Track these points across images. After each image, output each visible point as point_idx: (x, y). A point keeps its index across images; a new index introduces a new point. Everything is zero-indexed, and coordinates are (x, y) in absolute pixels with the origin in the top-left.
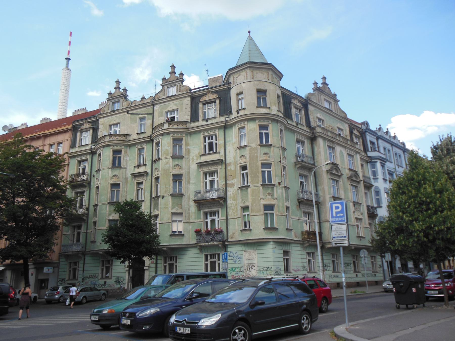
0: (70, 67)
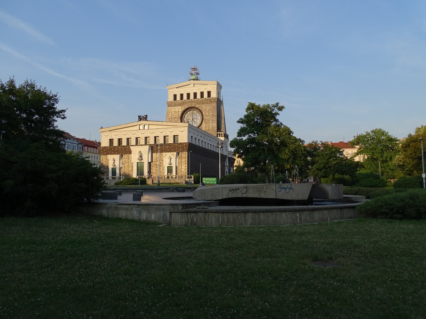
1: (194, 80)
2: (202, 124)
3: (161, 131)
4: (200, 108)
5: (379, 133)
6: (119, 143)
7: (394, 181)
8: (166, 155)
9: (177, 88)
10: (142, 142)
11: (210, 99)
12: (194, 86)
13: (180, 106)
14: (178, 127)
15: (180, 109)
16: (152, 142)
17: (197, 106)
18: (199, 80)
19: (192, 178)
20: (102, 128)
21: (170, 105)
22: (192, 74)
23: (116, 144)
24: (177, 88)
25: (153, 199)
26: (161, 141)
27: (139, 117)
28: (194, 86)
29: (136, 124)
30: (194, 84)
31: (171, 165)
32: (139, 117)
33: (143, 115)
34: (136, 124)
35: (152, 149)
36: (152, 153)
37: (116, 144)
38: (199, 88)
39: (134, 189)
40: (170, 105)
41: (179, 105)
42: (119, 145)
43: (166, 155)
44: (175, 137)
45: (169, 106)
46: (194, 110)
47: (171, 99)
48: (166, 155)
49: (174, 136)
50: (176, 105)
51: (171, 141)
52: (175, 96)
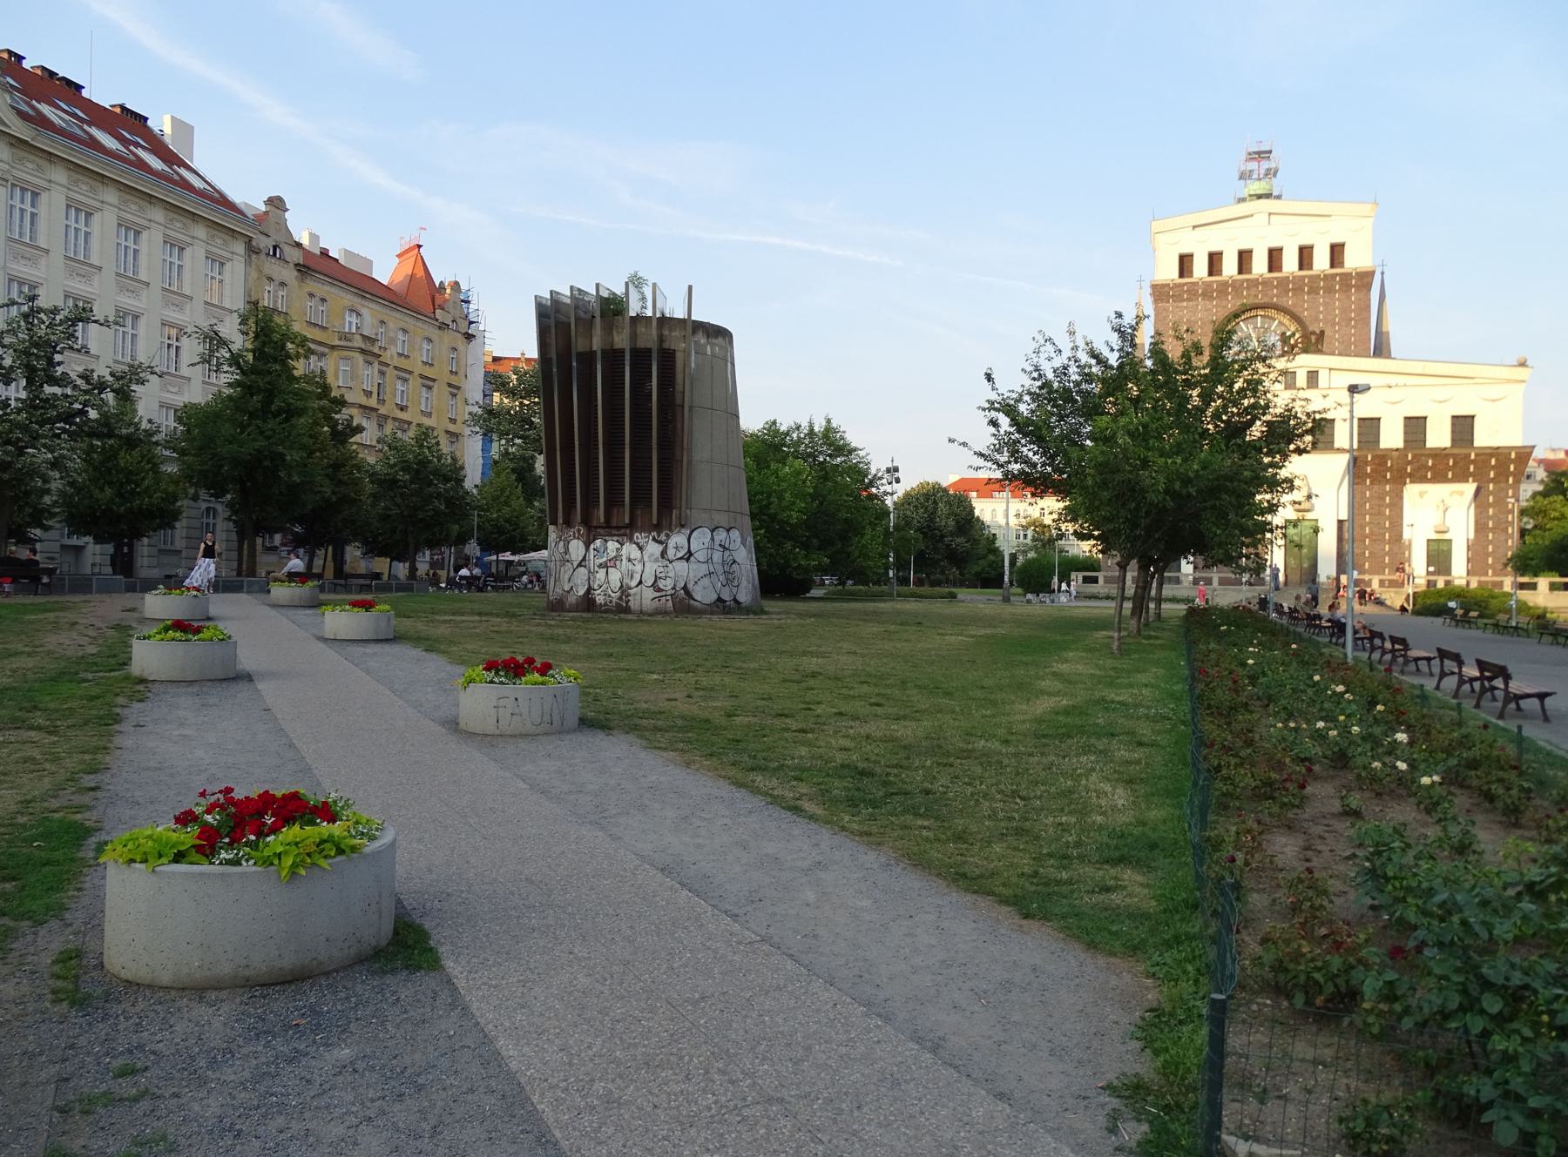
1: (1259, 197)
5: (831, 440)
7: (1479, 582)
9: (1194, 227)
11: (1193, 283)
14: (1475, 381)
18: (1279, 197)
19: (1211, 584)
20: (1523, 364)
22: (1243, 176)
24: (1194, 227)
26: (1392, 437)
30: (1270, 214)
31: (1446, 536)
39: (281, 603)
43: (1426, 492)
44: (1463, 426)
46: (1268, 317)
47: (1169, 272)
48: (1426, 492)
49: (1408, 420)
51: (1439, 436)
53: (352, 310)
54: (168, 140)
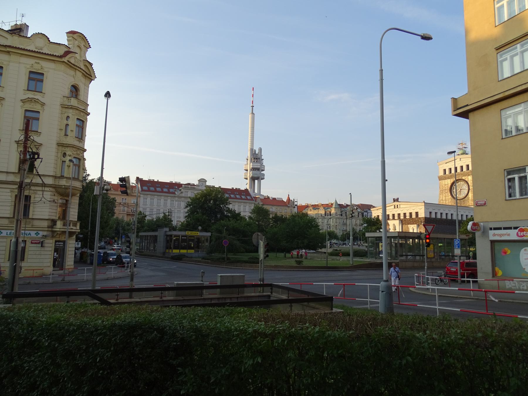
0: (254, 112)
2: (469, 194)
3: (407, 209)
4: (466, 180)
6: (417, 215)
8: (410, 226)
10: (396, 217)
12: (460, 160)
13: (449, 179)
15: (449, 182)
16: (402, 217)
17: (463, 178)
21: (440, 178)
23: (414, 216)
24: (446, 163)
25: (35, 107)
27: (394, 199)
28: (460, 160)
29: (391, 204)
30: (460, 159)
32: (394, 199)
33: (396, 198)
34: (391, 204)
35: (402, 222)
36: (402, 225)
37: (414, 216)
38: (464, 162)
40: (440, 178)
41: (448, 178)
42: (417, 217)
45: (440, 180)
47: (441, 173)
50: (445, 178)
52: (445, 170)
53: (271, 208)
54: (249, 192)
